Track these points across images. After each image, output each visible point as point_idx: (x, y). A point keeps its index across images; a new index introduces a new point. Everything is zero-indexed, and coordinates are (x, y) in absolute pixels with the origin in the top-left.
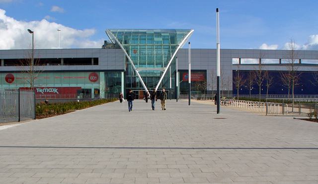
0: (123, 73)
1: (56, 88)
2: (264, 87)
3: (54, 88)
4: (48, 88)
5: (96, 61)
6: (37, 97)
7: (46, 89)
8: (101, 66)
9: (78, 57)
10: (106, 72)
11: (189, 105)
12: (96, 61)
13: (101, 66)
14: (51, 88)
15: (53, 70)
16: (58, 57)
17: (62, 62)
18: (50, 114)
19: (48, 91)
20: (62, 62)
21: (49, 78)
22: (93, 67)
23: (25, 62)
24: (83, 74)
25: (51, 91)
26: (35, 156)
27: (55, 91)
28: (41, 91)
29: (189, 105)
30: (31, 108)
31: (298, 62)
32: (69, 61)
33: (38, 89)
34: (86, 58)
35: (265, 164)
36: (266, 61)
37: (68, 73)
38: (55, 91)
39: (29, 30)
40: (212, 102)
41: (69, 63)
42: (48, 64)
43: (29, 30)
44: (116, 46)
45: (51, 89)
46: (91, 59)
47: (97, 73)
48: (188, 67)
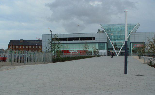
0: (106, 44)
1: (77, 50)
3: (76, 50)
4: (74, 50)
5: (94, 38)
6: (123, 50)
7: (73, 51)
9: (90, 37)
11: (126, 72)
12: (94, 38)
14: (75, 50)
15: (69, 42)
16: (78, 37)
17: (80, 39)
19: (74, 51)
20: (80, 39)
24: (82, 45)
25: (75, 52)
26: (57, 86)
27: (77, 51)
29: (126, 72)
30: (51, 59)
34: (84, 37)
37: (72, 44)
38: (77, 51)
39: (50, 31)
42: (74, 40)
43: (50, 31)
44: (103, 32)
46: (92, 37)
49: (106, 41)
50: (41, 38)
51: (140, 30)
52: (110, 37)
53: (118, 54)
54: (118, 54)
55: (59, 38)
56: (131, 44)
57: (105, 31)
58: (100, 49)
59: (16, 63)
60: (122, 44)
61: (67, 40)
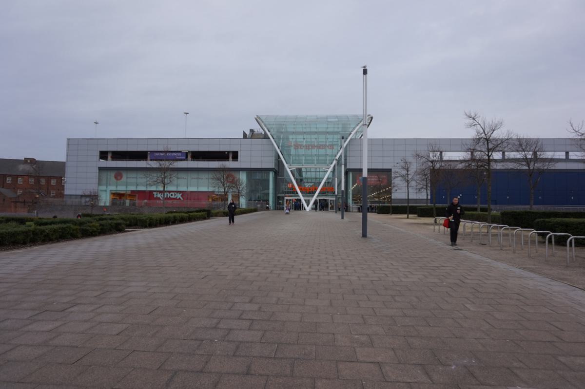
1: (180, 192)
2: (188, 198)
5: (235, 156)
8: (243, 162)
10: (250, 171)
12: (235, 156)
13: (243, 162)
17: (231, 156)
18: (197, 220)
19: (169, 195)
20: (231, 156)
21: (200, 178)
22: (230, 164)
23: (141, 155)
25: (173, 197)
27: (179, 196)
28: (159, 195)
31: (564, 157)
32: (198, 156)
33: (155, 193)
35: (562, 330)
36: (447, 156)
38: (179, 196)
40: (226, 220)
41: (203, 158)
45: (173, 194)
46: (146, 152)
47: (233, 173)
48: (361, 162)
49: (271, 165)
50: (52, 152)
51: (374, 132)
52: (285, 153)
53: (308, 206)
54: (308, 206)
55: (513, 159)
56: (351, 175)
57: (269, 134)
58: (334, 193)
59: (60, 239)
60: (318, 175)
61: (109, 158)
